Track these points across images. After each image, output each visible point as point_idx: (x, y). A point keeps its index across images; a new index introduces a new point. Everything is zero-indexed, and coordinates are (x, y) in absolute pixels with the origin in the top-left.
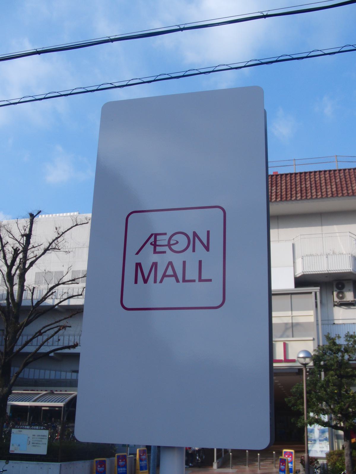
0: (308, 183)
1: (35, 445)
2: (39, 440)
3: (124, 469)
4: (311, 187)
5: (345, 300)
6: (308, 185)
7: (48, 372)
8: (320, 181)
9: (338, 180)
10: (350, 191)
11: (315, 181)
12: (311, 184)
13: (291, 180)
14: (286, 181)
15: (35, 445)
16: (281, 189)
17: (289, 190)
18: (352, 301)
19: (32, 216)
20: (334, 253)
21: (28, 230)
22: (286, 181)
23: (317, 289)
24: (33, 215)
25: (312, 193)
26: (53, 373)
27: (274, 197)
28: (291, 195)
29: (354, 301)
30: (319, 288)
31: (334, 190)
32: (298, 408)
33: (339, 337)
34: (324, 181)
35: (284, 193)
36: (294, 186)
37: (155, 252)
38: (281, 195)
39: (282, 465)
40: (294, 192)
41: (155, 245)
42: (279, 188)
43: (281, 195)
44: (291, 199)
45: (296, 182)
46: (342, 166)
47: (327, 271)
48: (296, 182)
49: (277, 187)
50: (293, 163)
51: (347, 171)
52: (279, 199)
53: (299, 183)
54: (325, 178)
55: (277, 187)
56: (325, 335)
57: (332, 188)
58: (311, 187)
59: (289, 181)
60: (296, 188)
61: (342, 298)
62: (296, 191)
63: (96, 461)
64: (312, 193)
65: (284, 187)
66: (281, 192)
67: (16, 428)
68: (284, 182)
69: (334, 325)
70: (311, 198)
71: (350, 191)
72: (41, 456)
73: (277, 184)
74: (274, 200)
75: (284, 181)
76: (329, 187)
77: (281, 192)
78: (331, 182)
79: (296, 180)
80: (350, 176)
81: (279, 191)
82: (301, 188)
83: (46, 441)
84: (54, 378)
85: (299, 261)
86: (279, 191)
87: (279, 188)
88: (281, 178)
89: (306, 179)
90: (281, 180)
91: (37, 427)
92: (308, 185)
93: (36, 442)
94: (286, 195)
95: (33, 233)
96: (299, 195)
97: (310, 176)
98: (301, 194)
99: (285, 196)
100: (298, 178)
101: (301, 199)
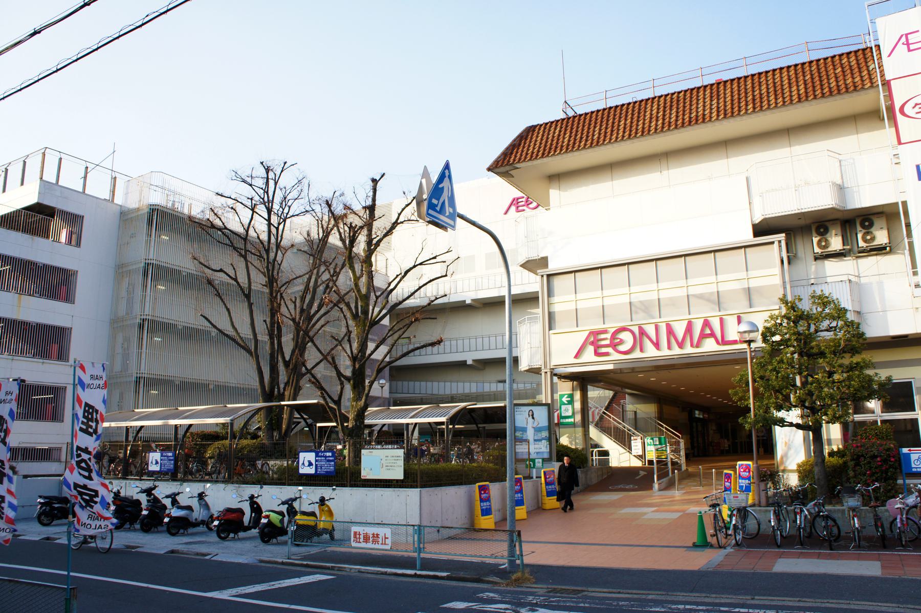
0: (764, 87)
1: (388, 468)
2: (394, 461)
3: (519, 495)
4: (768, 93)
5: (829, 249)
6: (764, 91)
7: (467, 385)
8: (782, 82)
9: (808, 77)
10: (826, 90)
11: (774, 83)
12: (768, 89)
13: (739, 87)
14: (732, 89)
15: (389, 468)
16: (725, 102)
17: (736, 101)
18: (840, 250)
19: (375, 181)
20: (807, 183)
21: (370, 199)
22: (732, 89)
23: (782, 236)
24: (376, 180)
25: (769, 101)
26: (474, 385)
27: (714, 114)
28: (740, 107)
29: (844, 249)
30: (784, 235)
31: (802, 91)
32: (746, 403)
33: (800, 300)
34: (787, 81)
35: (729, 107)
36: (743, 95)
37: (518, 211)
38: (725, 110)
39: (727, 481)
40: (743, 104)
41: (597, 347)
42: (721, 100)
43: (725, 110)
44: (739, 114)
45: (746, 89)
46: (814, 56)
47: (799, 210)
48: (746, 89)
49: (718, 99)
50: (743, 62)
51: (822, 61)
52: (722, 116)
53: (750, 89)
54: (789, 76)
55: (718, 99)
56: (779, 298)
57: (798, 90)
58: (768, 93)
59: (736, 88)
60: (746, 97)
61: (826, 247)
62: (747, 102)
63: (479, 486)
64: (769, 101)
65: (729, 99)
66: (725, 106)
67: (366, 449)
68: (728, 91)
69: (813, 286)
70: (769, 108)
71: (826, 90)
72: (397, 481)
73: (718, 96)
74: (715, 118)
75: (729, 90)
76: (794, 88)
77: (725, 106)
78: (797, 82)
79: (746, 85)
80: (826, 68)
81: (721, 104)
82: (754, 96)
83: (401, 463)
84: (475, 391)
85: (756, 200)
86: (721, 104)
87: (721, 100)
88: (725, 86)
89: (760, 83)
90: (725, 90)
91: (390, 446)
92: (764, 91)
93: (390, 465)
94: (732, 109)
95: (377, 202)
96: (750, 106)
97: (767, 77)
98: (754, 104)
99: (730, 110)
100: (749, 82)
101: (754, 111)
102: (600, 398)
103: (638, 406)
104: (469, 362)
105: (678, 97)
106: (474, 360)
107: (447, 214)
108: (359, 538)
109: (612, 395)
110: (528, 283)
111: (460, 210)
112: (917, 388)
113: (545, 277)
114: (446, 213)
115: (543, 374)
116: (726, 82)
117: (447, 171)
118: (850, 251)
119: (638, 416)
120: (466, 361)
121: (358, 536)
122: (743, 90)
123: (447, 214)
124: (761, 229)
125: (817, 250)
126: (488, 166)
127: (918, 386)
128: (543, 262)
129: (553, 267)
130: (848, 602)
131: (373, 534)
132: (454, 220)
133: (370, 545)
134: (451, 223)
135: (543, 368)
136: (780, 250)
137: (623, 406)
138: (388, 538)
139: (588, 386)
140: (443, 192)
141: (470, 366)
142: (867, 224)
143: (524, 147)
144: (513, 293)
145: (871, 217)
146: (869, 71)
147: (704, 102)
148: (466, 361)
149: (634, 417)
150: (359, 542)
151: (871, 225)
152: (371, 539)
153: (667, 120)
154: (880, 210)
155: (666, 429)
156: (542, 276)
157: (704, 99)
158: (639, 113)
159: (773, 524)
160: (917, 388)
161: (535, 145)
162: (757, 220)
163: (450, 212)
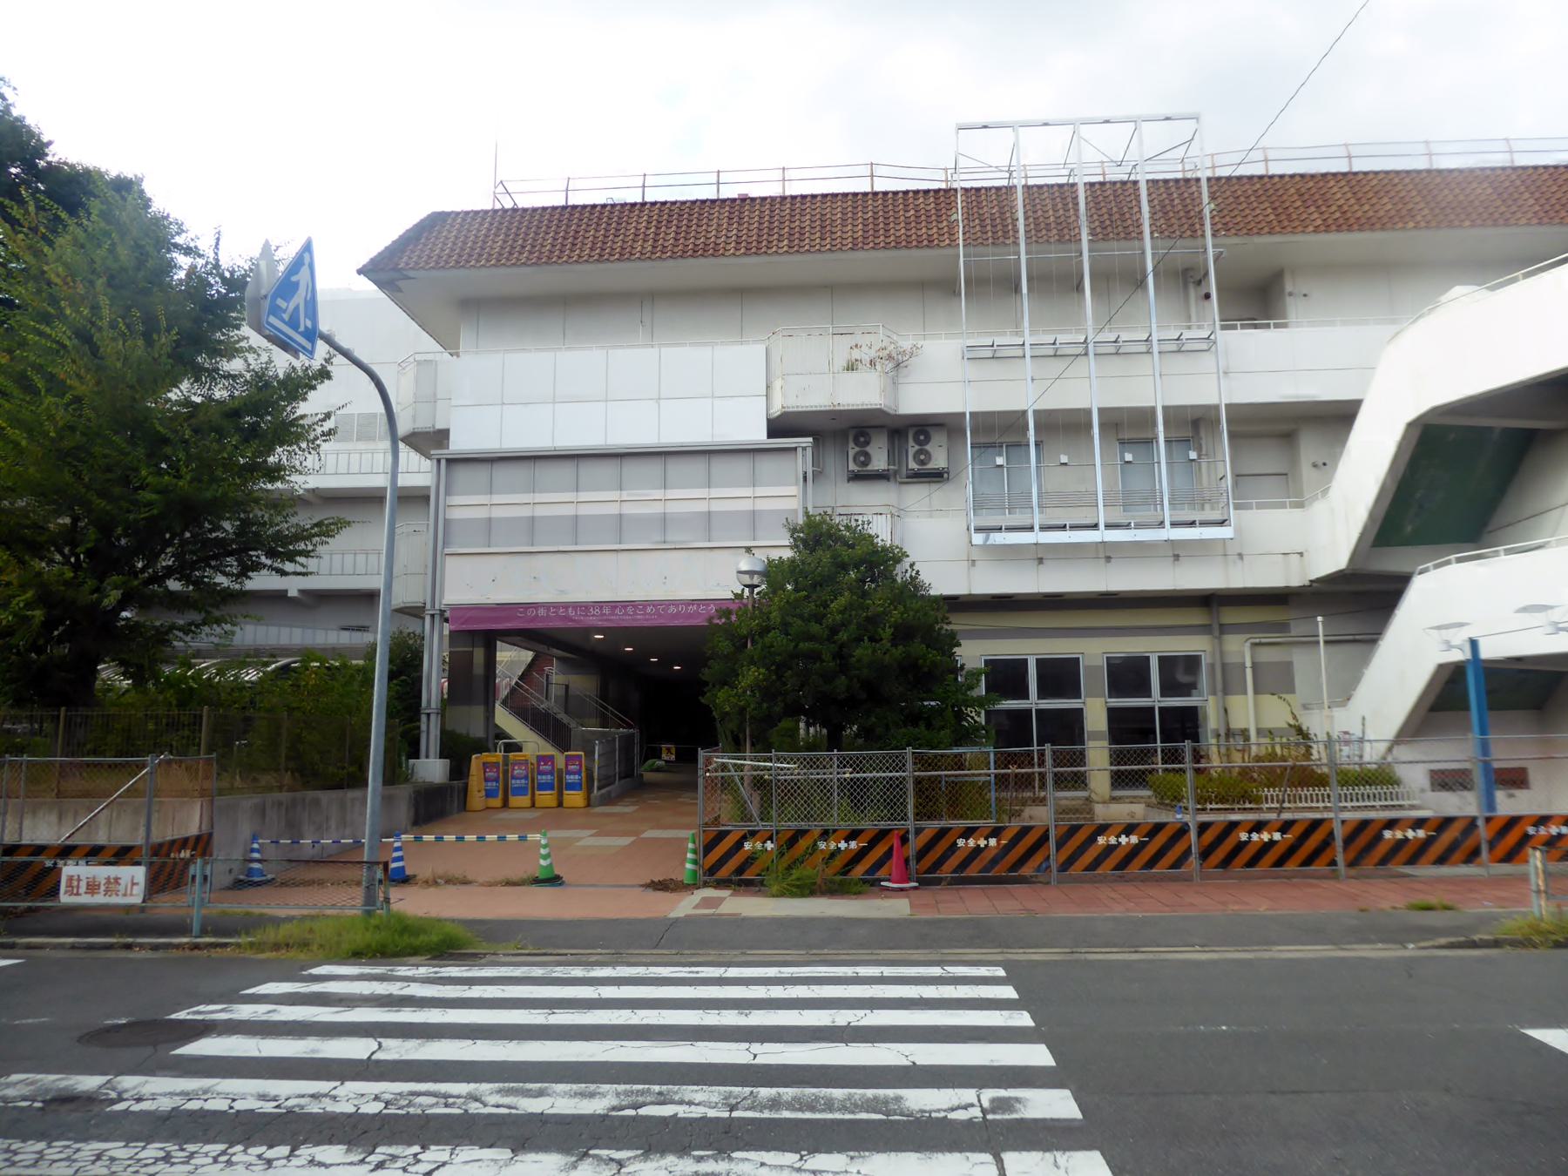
5: (869, 468)
30: (810, 439)
61: (865, 464)
102: (512, 663)
103: (570, 677)
104: (293, 593)
106: (301, 591)
107: (302, 329)
108: (78, 887)
109: (530, 659)
110: (417, 471)
111: (324, 327)
112: (1086, 668)
114: (299, 327)
115: (428, 619)
116: (753, 199)
117: (306, 256)
118: (896, 473)
119: (570, 692)
120: (286, 591)
121: (75, 883)
123: (302, 329)
124: (778, 427)
126: (364, 260)
127: (1087, 663)
128: (441, 437)
129: (460, 443)
131: (108, 879)
132: (313, 343)
133: (99, 899)
134: (308, 346)
135: (428, 606)
136: (804, 462)
137: (547, 675)
138: (137, 884)
139: (498, 643)
140: (297, 289)
141: (293, 599)
142: (922, 437)
144: (400, 483)
145: (929, 429)
148: (286, 591)
149: (564, 693)
150: (78, 894)
151: (928, 440)
152: (103, 888)
154: (941, 421)
155: (612, 713)
156: (439, 461)
160: (1085, 667)
162: (776, 411)
163: (306, 327)
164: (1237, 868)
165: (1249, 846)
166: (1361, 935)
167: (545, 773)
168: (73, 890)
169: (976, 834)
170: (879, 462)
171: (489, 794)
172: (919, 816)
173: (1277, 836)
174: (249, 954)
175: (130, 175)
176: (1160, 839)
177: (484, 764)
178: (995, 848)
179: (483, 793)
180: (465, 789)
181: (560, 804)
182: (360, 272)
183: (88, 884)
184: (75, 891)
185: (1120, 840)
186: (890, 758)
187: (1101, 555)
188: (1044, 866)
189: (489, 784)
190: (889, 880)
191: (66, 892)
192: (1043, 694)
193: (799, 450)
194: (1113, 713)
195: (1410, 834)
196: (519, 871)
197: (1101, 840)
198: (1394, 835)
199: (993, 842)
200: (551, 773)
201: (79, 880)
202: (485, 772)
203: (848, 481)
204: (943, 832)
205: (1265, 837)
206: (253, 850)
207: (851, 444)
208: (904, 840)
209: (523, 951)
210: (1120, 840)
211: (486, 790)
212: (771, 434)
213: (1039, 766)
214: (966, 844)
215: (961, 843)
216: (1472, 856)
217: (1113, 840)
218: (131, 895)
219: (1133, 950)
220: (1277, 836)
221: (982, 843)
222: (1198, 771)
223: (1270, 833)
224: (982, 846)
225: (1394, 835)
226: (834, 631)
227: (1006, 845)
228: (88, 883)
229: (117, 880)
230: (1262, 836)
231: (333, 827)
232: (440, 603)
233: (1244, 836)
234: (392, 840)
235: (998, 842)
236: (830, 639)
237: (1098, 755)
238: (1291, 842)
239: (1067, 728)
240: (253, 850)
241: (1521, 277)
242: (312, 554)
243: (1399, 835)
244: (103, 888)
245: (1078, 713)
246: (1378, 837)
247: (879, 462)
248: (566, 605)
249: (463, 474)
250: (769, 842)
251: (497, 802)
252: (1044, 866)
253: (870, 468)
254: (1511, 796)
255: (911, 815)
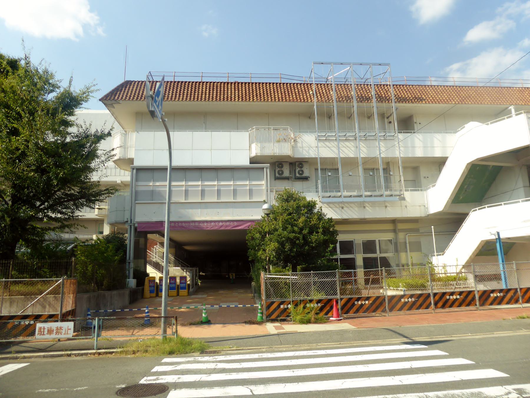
5: (283, 175)
14: (245, 87)
27: (135, 98)
28: (250, 97)
30: (269, 165)
61: (301, 174)
79: (252, 87)
105: (217, 85)
108: (44, 332)
113: (135, 171)
121: (42, 330)
122: (201, 91)
124: (253, 161)
125: (297, 175)
128: (131, 161)
130: (300, 345)
138: (70, 329)
143: (124, 92)
145: (303, 163)
146: (310, 94)
147: (231, 91)
150: (44, 334)
151: (282, 167)
152: (55, 331)
153: (211, 95)
157: (231, 89)
158: (195, 88)
159: (199, 307)
161: (132, 92)
162: (253, 154)
164: (361, 314)
165: (408, 303)
166: (500, 328)
167: (173, 284)
168: (41, 333)
169: (284, 304)
170: (286, 173)
171: (151, 292)
172: (341, 294)
173: (458, 297)
174: (123, 356)
175: (17, 58)
176: (421, 300)
177: (149, 280)
178: (368, 304)
179: (149, 291)
180: (143, 289)
181: (178, 295)
182: (100, 100)
183: (48, 330)
184: (42, 333)
185: (409, 300)
186: (315, 274)
187: (362, 206)
188: (384, 310)
189: (151, 288)
190: (332, 317)
191: (38, 334)
192: (342, 253)
193: (265, 169)
194: (365, 259)
195: (499, 295)
196: (198, 320)
197: (403, 300)
198: (494, 295)
199: (367, 302)
200: (154, 286)
201: (44, 329)
202: (149, 284)
203: (275, 180)
204: (350, 299)
205: (455, 297)
206: (88, 315)
207: (277, 168)
208: (337, 302)
209: (232, 349)
210: (409, 300)
211: (150, 290)
212: (250, 163)
213: (354, 277)
214: (358, 303)
215: (356, 303)
216: (517, 301)
217: (406, 300)
218: (67, 334)
219: (450, 336)
220: (458, 297)
221: (363, 303)
222: (308, 284)
223: (456, 296)
224: (363, 304)
225: (494, 295)
226: (301, 229)
227: (371, 303)
228: (48, 330)
229: (61, 328)
230: (454, 297)
231: (109, 305)
232: (134, 221)
233: (448, 297)
234: (145, 309)
235: (368, 302)
236: (300, 233)
237: (360, 272)
238: (463, 298)
239: (350, 264)
240: (88, 315)
241: (506, 118)
242: (104, 201)
243: (495, 295)
244: (55, 331)
245: (353, 260)
246: (489, 296)
247: (286, 173)
248: (182, 222)
249: (142, 174)
250: (289, 305)
251: (154, 295)
252: (384, 310)
253: (283, 175)
254: (499, 283)
255: (339, 293)
